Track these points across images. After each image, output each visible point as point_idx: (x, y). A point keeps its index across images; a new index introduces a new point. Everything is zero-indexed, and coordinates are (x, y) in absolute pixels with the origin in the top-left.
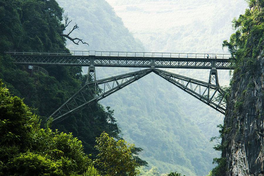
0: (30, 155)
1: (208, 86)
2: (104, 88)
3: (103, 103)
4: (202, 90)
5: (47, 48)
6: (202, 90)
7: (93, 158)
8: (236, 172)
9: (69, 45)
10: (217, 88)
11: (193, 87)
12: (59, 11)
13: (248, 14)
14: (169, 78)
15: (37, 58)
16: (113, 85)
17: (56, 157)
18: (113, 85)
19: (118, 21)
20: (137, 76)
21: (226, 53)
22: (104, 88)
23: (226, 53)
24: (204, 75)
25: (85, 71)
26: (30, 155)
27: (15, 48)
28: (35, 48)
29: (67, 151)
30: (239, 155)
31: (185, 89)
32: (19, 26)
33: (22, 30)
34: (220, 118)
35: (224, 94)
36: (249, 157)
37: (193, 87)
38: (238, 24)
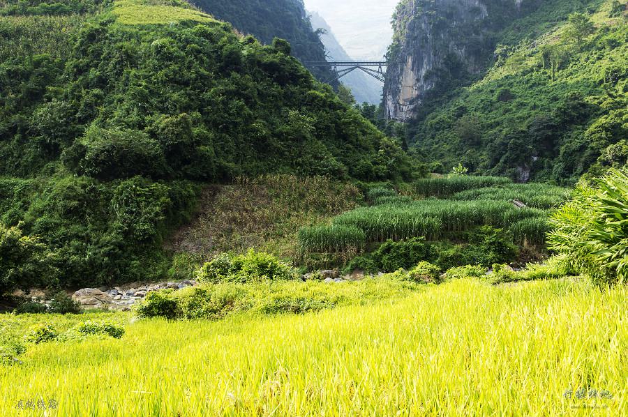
0: (313, 91)
1: (378, 72)
2: (340, 74)
3: (339, 79)
4: (376, 74)
5: (319, 60)
6: (376, 74)
7: (337, 93)
8: (240, 372)
9: (327, 58)
10: (381, 73)
11: (372, 72)
12: (323, 46)
13: (393, 44)
14: (363, 69)
15: (315, 63)
16: (343, 73)
17: (323, 92)
18: (343, 73)
19: (344, 52)
20: (352, 69)
21: (384, 60)
22: (340, 74)
23: (384, 60)
24: (376, 68)
25: (333, 68)
26: (313, 91)
27: (308, 60)
28: (314, 59)
29: (327, 90)
30: (390, 97)
31: (369, 73)
32: (309, 52)
33: (310, 53)
34: (383, 84)
35: (384, 75)
36: (393, 98)
37: (372, 72)
38: (389, 48)
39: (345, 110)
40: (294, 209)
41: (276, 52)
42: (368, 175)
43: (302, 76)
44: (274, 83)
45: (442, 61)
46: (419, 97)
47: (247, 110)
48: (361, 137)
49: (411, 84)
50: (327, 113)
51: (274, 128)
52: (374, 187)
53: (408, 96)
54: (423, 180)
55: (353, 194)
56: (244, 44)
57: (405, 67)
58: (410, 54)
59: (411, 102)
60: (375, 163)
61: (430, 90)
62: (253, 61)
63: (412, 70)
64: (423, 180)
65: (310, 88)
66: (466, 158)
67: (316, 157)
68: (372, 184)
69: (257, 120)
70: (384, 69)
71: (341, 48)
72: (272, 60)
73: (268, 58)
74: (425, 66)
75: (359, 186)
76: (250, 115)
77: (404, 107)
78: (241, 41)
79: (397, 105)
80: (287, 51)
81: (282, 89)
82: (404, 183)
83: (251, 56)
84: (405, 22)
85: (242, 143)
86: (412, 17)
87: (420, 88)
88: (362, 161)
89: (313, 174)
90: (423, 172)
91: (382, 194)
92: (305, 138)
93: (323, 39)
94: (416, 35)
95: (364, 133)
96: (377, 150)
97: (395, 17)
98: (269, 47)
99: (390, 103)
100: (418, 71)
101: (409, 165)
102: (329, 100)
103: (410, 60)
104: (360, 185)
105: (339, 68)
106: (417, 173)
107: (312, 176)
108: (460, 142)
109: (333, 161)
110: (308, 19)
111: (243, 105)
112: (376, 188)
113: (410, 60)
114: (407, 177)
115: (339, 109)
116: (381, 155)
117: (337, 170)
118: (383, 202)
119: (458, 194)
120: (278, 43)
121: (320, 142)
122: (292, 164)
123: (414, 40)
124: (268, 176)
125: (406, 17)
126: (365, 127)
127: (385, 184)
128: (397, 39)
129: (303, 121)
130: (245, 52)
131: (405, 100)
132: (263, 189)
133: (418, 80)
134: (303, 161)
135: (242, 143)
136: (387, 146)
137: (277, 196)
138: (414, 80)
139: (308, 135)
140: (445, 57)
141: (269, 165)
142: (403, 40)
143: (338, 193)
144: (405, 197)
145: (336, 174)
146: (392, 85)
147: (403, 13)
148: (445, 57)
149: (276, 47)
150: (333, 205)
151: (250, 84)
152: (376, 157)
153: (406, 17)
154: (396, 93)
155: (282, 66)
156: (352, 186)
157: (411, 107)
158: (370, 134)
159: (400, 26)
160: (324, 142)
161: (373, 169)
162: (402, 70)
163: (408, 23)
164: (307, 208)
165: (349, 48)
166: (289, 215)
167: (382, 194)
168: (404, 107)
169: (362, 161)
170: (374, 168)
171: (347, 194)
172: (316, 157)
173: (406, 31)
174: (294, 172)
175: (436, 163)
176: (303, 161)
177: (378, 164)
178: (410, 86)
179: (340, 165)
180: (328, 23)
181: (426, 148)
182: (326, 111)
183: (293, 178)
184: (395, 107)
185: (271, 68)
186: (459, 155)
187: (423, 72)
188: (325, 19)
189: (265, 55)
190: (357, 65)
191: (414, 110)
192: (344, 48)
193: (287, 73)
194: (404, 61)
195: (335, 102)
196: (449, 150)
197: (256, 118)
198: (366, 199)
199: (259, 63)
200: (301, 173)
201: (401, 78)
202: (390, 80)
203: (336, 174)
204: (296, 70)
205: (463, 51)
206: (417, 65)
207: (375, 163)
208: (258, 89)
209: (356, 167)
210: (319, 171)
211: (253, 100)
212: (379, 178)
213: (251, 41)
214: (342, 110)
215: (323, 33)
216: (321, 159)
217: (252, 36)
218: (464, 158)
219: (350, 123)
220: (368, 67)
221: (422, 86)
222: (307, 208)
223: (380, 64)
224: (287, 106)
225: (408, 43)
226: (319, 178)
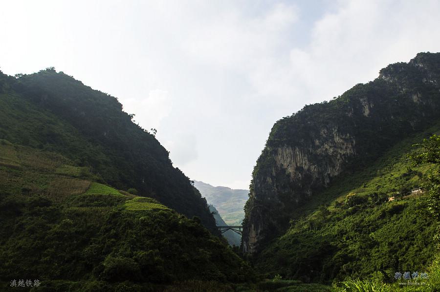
0: (210, 240)
14: (233, 230)
21: (242, 225)
23: (242, 225)
26: (210, 240)
41: (194, 222)
52: (239, 286)
54: (262, 282)
59: (254, 245)
64: (262, 282)
68: (238, 284)
70: (242, 229)
73: (191, 225)
75: (232, 286)
79: (248, 245)
80: (199, 222)
83: (183, 224)
87: (258, 238)
88: (233, 273)
93: (215, 216)
95: (234, 259)
102: (218, 244)
103: (253, 226)
105: (222, 229)
106: (259, 279)
107: (209, 280)
109: (219, 273)
110: (208, 208)
113: (253, 226)
127: (244, 284)
128: (246, 216)
129: (206, 253)
131: (251, 244)
133: (257, 235)
136: (244, 266)
139: (208, 260)
142: (249, 216)
146: (245, 235)
154: (247, 241)
162: (250, 230)
175: (267, 274)
184: (247, 247)
191: (256, 248)
194: (250, 226)
206: (256, 228)
213: (183, 217)
216: (214, 272)
221: (259, 237)
223: (240, 227)
225: (252, 218)
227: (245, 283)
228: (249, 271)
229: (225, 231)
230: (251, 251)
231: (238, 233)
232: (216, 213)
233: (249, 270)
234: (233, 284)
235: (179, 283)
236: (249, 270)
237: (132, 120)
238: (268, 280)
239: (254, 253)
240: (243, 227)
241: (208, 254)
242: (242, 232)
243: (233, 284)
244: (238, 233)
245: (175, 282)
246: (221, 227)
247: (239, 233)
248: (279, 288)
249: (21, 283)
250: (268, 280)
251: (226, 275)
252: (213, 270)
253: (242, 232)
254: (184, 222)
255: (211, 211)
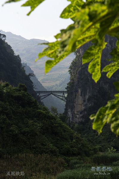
0: (39, 110)
4: (61, 97)
10: (64, 97)
12: (32, 83)
13: (70, 82)
14: (55, 95)
16: (43, 97)
18: (43, 97)
21: (66, 90)
23: (66, 90)
25: (38, 94)
26: (39, 110)
30: (69, 110)
31: (58, 97)
34: (65, 103)
39: (55, 120)
40: (33, 172)
41: (20, 91)
42: (68, 153)
43: (33, 102)
44: (20, 106)
45: (96, 91)
46: (85, 110)
47: (8, 121)
48: (63, 133)
49: (81, 103)
50: (47, 121)
51: (21, 130)
52: (72, 159)
53: (79, 109)
54: (96, 155)
55: (62, 163)
56: (4, 87)
57: (77, 94)
58: (80, 87)
59: (81, 113)
60: (72, 147)
61: (90, 106)
62: (9, 95)
63: (81, 95)
64: (96, 155)
65: (37, 108)
66: (113, 143)
67: (42, 145)
68: (71, 158)
69: (13, 125)
70: (66, 95)
71: (39, 82)
72: (18, 94)
73: (17, 94)
74: (88, 93)
75: (65, 159)
76: (9, 123)
77: (77, 116)
78: (2, 85)
79: (73, 114)
80: (25, 90)
81: (24, 109)
82: (86, 157)
83: (8, 92)
84: (77, 71)
85: (6, 137)
86: (80, 68)
87: (86, 105)
88: (65, 146)
89: (41, 153)
90: (95, 151)
91: (76, 163)
92: (37, 134)
93: (32, 78)
94: (82, 78)
95: (65, 131)
96: (72, 140)
97: (71, 68)
98: (16, 88)
99: (70, 113)
100: (84, 96)
101: (88, 148)
102: (47, 114)
103: (80, 91)
104: (65, 158)
105: (41, 95)
106: (92, 152)
107: (41, 154)
108: (109, 134)
109: (51, 145)
110: (23, 68)
111: (6, 118)
112: (74, 160)
113: (80, 91)
114: (87, 154)
115: (52, 119)
116: (74, 142)
117: (53, 151)
118: (78, 167)
119: (114, 163)
120: (21, 86)
121: (44, 136)
122: (30, 147)
123: (81, 80)
124: (20, 155)
125: (77, 68)
126: (65, 128)
127: (77, 158)
128: (72, 79)
129: (36, 125)
130: (5, 91)
131: (78, 112)
132: (17, 161)
133: (84, 101)
134: (36, 147)
135: (6, 137)
136: (77, 138)
137: (25, 165)
138: (82, 101)
139: (38, 133)
140: (98, 89)
141: (19, 148)
142: (76, 80)
143: (55, 163)
144: (88, 164)
145: (53, 152)
146: (70, 102)
147: (75, 66)
148: (98, 89)
149: (20, 88)
150: (53, 169)
151: (8, 107)
152: (72, 144)
153: (77, 68)
154: (73, 108)
155: (23, 98)
156: (61, 159)
157: (81, 115)
158: (68, 131)
159: (74, 73)
160: (46, 136)
161: (71, 150)
162: (76, 96)
163: (78, 71)
164: (40, 171)
165: (43, 82)
166: (32, 175)
167: (76, 163)
168: (77, 116)
169: (65, 146)
170: (71, 149)
171: (59, 163)
172: (42, 145)
173: (77, 75)
174: (32, 152)
175: (98, 147)
176: (36, 147)
177: (73, 147)
178: (80, 104)
179: (55, 148)
180: (32, 69)
181: (91, 138)
182: (46, 120)
183: (32, 155)
184: (73, 115)
185: (18, 99)
186: (109, 142)
187: (87, 97)
188: (31, 67)
189: (15, 92)
190: (51, 93)
191: (82, 117)
192: (41, 82)
193: (26, 101)
194: (77, 91)
195: (50, 115)
196: (104, 139)
197: (12, 124)
198: (68, 166)
199: (12, 96)
200: (35, 153)
201: (75, 100)
202: (69, 101)
203: (53, 152)
204: (30, 99)
205: (107, 86)
206: (83, 94)
207: (72, 147)
208: (12, 110)
209: (62, 149)
210: (44, 151)
211: (10, 115)
212: (74, 155)
213: (7, 85)
214: (54, 119)
215: (32, 76)
216: (45, 145)
217: (7, 83)
218: (112, 143)
219: (58, 126)
220: (58, 94)
221: (87, 104)
222: (40, 171)
223: (63, 92)
224: (26, 118)
225: (78, 81)
226: (45, 156)
227: (79, 156)
228: (82, 143)
229: (45, 97)
230: (77, 120)
231: (61, 99)
232: (32, 75)
233: (82, 142)
234: (66, 158)
235: (9, 157)
236: (82, 142)
237: (107, 75)
238: (101, 154)
239: (81, 123)
240: (67, 92)
241: (39, 125)
242: (66, 98)
243: (66, 158)
244: (61, 99)
245: (5, 156)
246: (40, 92)
247: (62, 99)
248: (116, 161)
249: (13, 173)
250: (101, 154)
251: (58, 148)
252: (44, 143)
253: (66, 98)
254: (9, 90)
255: (27, 73)
